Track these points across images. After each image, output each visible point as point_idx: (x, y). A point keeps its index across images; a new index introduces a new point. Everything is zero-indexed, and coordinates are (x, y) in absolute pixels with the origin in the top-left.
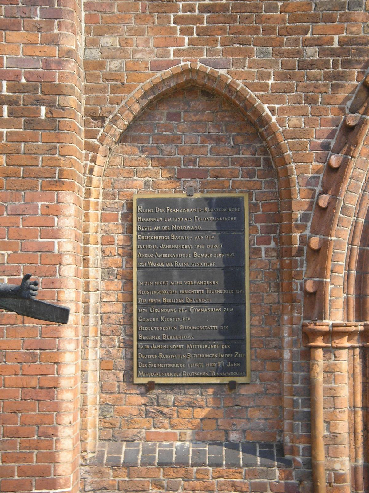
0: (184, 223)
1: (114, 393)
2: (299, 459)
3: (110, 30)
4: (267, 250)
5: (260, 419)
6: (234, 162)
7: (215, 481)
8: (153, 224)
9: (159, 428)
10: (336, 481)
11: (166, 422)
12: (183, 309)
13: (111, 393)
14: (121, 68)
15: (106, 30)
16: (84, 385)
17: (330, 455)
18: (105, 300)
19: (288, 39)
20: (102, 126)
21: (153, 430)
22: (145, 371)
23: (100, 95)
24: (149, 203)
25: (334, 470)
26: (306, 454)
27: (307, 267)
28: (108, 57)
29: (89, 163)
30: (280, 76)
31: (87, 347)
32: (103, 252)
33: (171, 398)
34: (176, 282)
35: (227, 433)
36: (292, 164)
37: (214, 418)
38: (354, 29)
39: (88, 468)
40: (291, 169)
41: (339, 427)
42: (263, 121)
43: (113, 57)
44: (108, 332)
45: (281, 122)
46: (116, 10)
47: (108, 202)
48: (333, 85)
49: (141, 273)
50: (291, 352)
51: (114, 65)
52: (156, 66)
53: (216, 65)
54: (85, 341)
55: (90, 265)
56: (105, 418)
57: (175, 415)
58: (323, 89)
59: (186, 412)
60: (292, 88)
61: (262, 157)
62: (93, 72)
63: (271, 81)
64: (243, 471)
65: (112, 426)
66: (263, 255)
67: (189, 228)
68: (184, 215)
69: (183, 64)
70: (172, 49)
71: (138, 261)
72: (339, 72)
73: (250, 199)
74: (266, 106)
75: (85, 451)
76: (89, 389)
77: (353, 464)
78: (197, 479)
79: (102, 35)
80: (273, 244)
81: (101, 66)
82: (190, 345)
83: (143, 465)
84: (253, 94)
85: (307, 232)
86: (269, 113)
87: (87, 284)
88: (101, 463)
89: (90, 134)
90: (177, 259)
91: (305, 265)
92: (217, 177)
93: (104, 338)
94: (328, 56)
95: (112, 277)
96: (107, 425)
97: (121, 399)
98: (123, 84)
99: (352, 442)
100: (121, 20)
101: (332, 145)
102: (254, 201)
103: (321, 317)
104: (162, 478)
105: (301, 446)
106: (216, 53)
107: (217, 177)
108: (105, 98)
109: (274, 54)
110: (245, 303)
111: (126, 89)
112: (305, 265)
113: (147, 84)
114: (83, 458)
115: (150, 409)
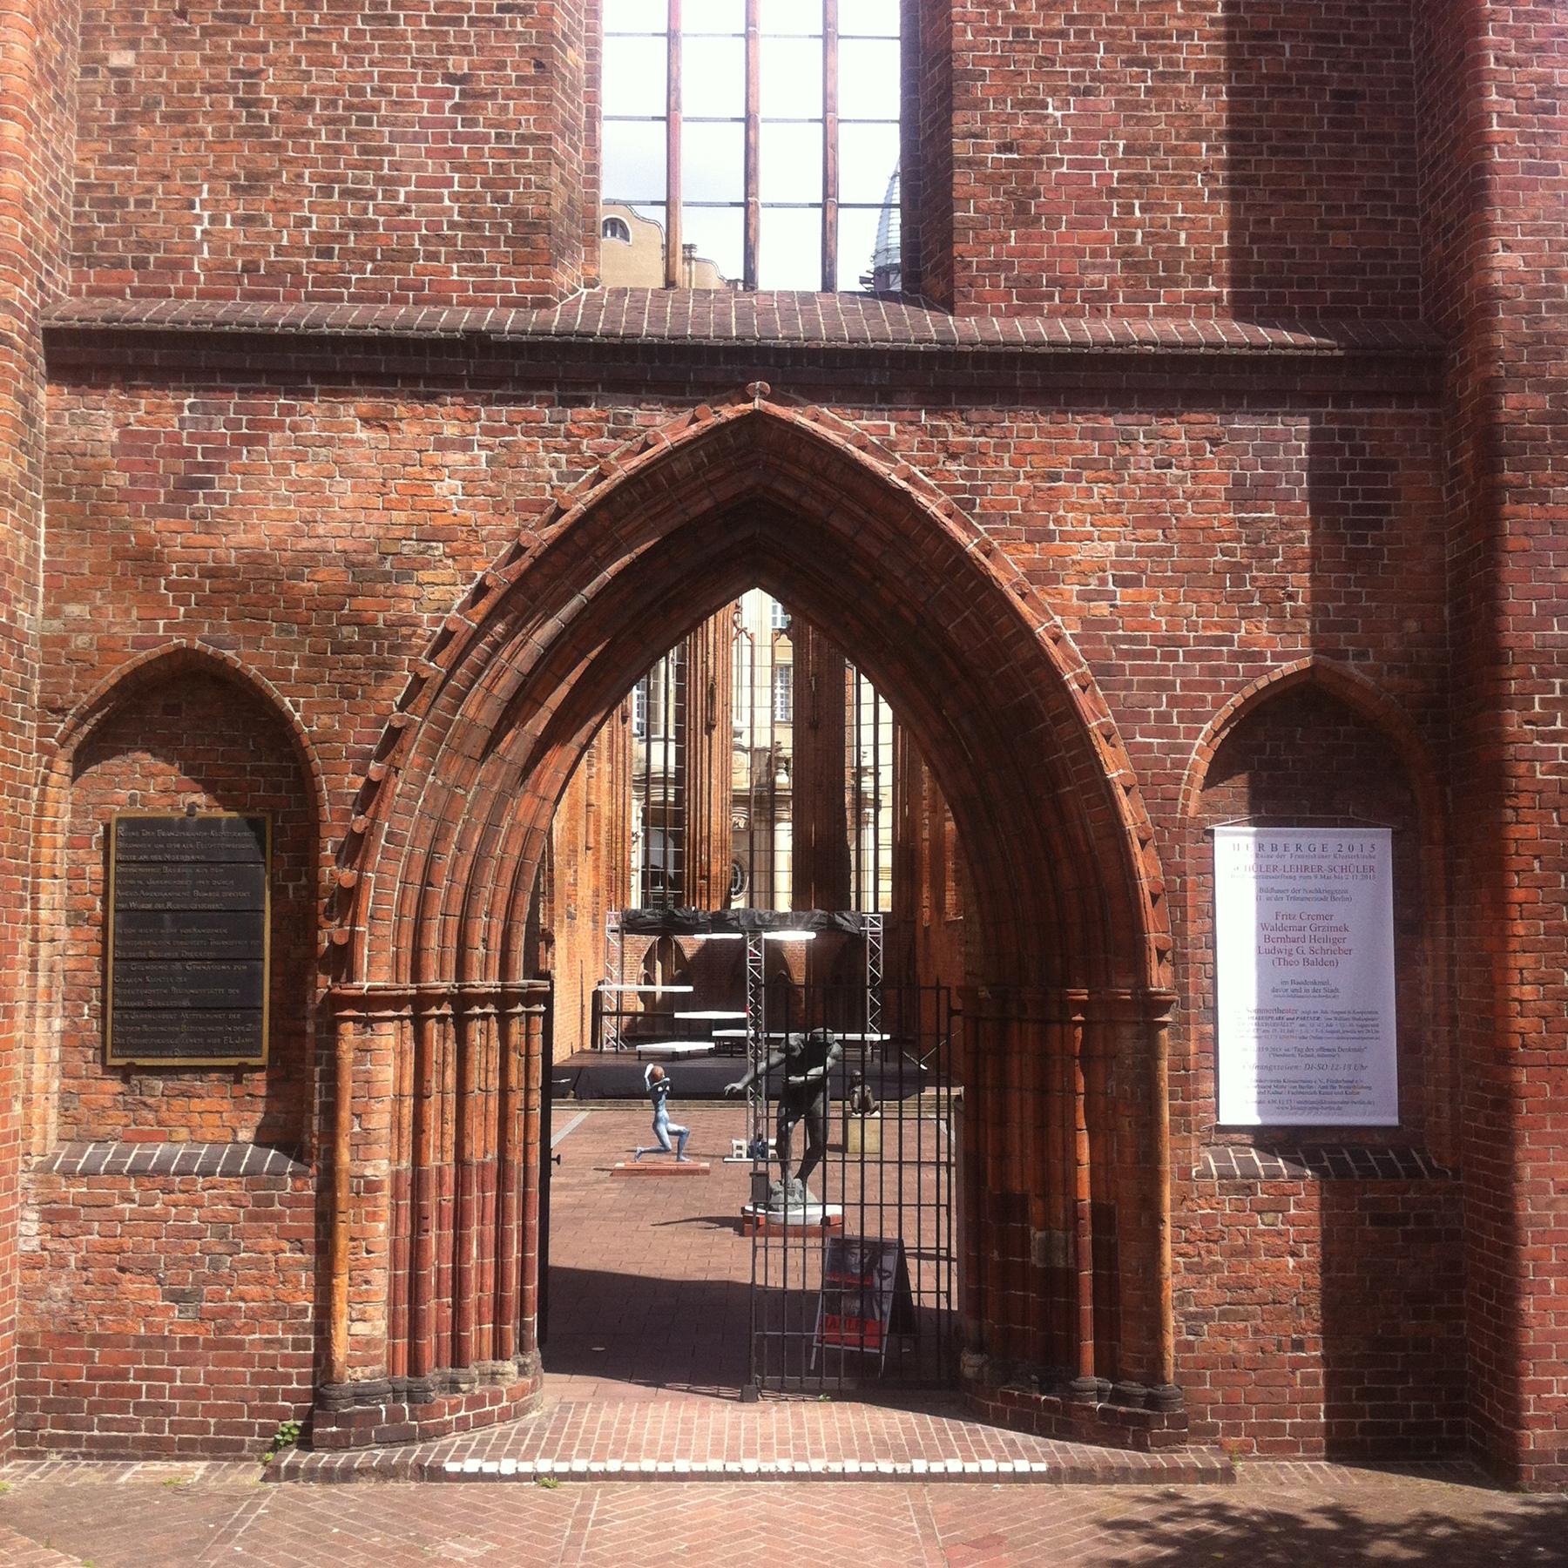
0: (182, 852)
1: (81, 1078)
3: (77, 598)
5: (280, 1112)
6: (256, 771)
7: (206, 1194)
8: (139, 852)
9: (142, 1124)
10: (367, 1190)
11: (151, 1116)
12: (178, 965)
13: (75, 1078)
14: (91, 644)
15: (72, 595)
16: (29, 1066)
17: (361, 1157)
18: (70, 952)
20: (62, 721)
21: (133, 1127)
22: (122, 1048)
23: (61, 680)
24: (133, 824)
25: (363, 1177)
28: (74, 631)
29: (42, 769)
30: (308, 662)
31: (34, 1016)
32: (70, 888)
33: (159, 1085)
34: (169, 929)
35: (235, 1132)
37: (217, 1112)
38: (403, 606)
39: (32, 1176)
40: (320, 782)
41: (373, 1121)
42: (283, 720)
43: (81, 631)
44: (73, 996)
45: (308, 721)
46: (86, 571)
47: (77, 821)
49: (120, 916)
50: (316, 1024)
51: (80, 641)
52: (140, 644)
53: (220, 645)
54: (31, 1008)
55: (41, 905)
56: (67, 1110)
57: (164, 1107)
59: (179, 1103)
60: (322, 677)
62: (53, 649)
63: (296, 667)
64: (244, 1180)
65: (77, 1121)
67: (187, 858)
68: (182, 840)
69: (176, 641)
70: (161, 623)
71: (117, 901)
73: (274, 820)
74: (287, 700)
75: (29, 1154)
76: (36, 1073)
77: (394, 1168)
78: (183, 1192)
79: (67, 603)
81: (63, 641)
82: (185, 1015)
83: (107, 1172)
84: (270, 684)
87: (35, 932)
88: (50, 1169)
89: (45, 731)
90: (170, 899)
92: (229, 791)
93: (67, 1003)
95: (80, 922)
96: (69, 1120)
97: (89, 1086)
98: (92, 665)
99: (395, 1140)
100: (93, 585)
102: (280, 824)
103: (350, 979)
104: (133, 1189)
106: (221, 628)
107: (229, 791)
108: (67, 684)
109: (300, 633)
110: (263, 960)
111: (97, 673)
113: (126, 666)
114: (26, 1162)
115: (129, 1099)
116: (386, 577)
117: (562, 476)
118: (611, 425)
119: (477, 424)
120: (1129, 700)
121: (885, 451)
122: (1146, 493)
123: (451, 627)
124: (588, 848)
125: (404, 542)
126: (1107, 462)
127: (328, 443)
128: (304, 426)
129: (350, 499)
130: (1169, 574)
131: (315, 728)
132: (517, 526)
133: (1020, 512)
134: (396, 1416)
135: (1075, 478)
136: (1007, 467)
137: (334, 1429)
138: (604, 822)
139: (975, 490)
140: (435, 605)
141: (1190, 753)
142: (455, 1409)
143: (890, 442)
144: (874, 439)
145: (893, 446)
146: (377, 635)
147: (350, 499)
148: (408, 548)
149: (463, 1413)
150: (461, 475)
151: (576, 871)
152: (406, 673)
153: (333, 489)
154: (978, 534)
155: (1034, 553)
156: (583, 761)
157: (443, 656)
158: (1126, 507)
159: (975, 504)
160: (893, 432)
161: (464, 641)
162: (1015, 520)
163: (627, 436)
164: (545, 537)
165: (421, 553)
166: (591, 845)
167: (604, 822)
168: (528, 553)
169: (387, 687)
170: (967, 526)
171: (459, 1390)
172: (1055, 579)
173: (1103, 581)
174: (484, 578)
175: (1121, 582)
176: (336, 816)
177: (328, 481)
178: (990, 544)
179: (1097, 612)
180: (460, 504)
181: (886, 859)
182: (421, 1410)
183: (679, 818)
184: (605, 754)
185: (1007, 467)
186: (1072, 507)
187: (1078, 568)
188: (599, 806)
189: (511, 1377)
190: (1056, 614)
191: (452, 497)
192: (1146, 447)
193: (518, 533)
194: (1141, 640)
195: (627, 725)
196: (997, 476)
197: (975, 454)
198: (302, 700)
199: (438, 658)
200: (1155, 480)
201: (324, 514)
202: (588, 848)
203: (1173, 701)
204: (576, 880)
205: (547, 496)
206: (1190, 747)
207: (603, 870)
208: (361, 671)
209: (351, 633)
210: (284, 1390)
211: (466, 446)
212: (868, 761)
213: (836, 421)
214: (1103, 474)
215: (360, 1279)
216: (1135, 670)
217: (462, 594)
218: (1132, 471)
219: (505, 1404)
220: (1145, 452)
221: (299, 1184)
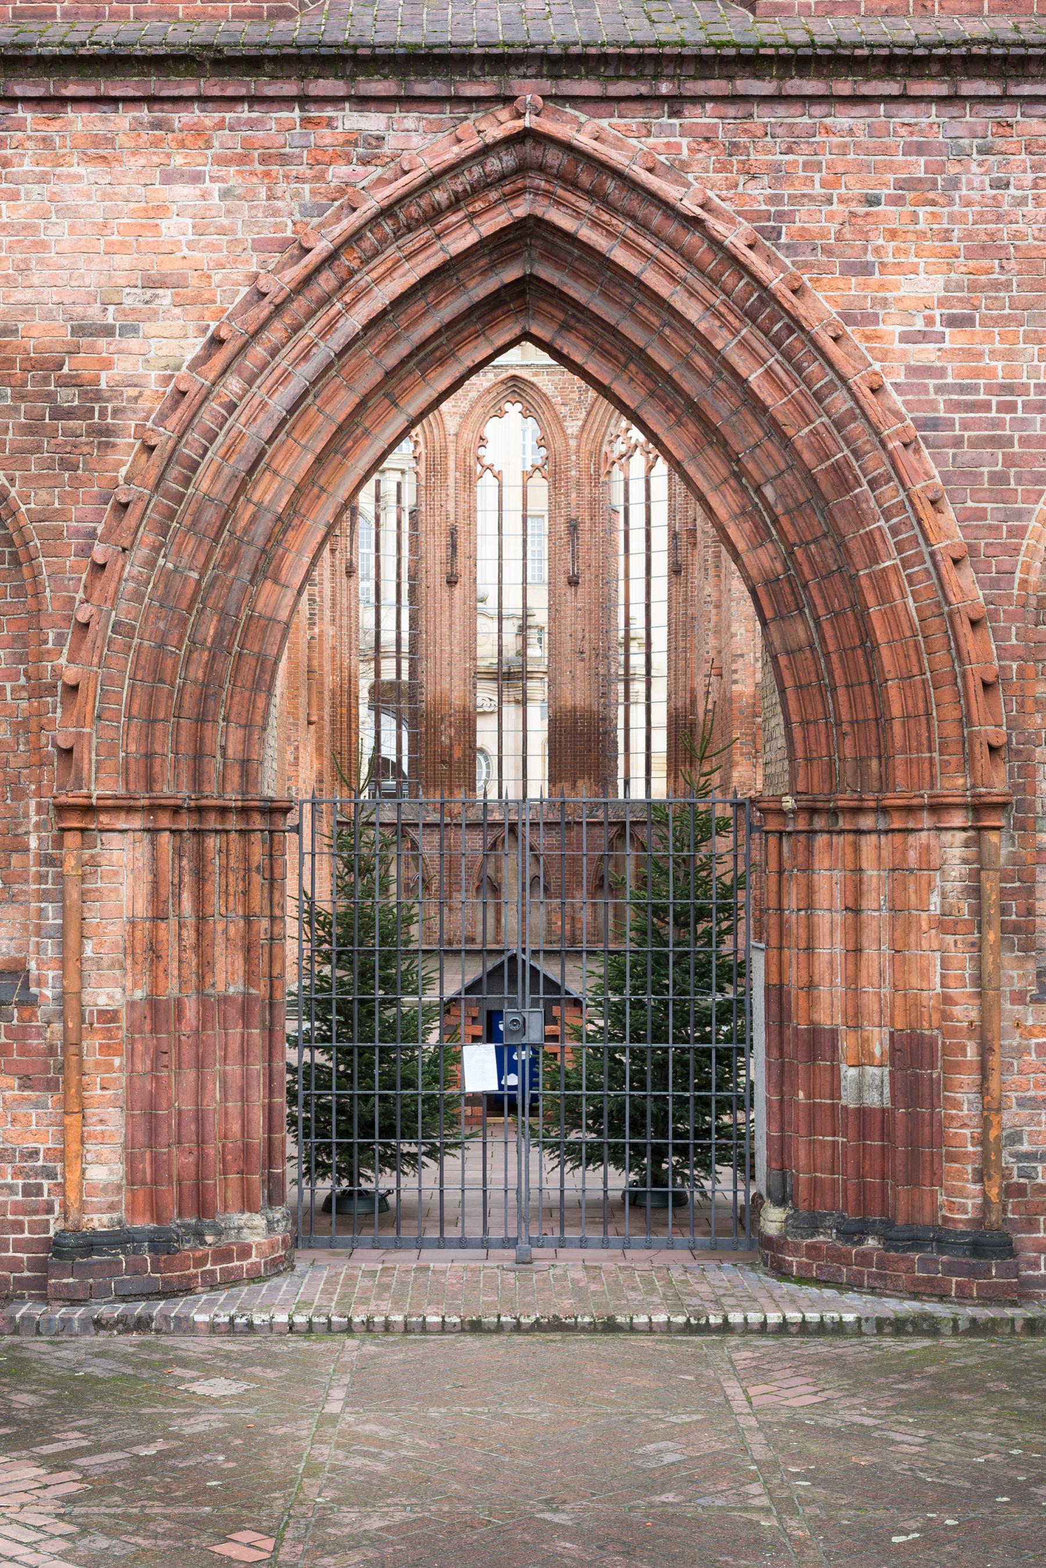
2: (48, 992)
4: (13, 690)
19: (33, 377)
26: (58, 985)
27: (63, 713)
35: (499, 1316)
36: (41, 559)
48: (99, 443)
50: (39, 838)
58: (86, 449)
61: (7, 550)
66: (9, 697)
72: (107, 425)
80: (23, 681)
85: (63, 661)
86: (7, 484)
91: (59, 710)
94: (91, 400)
101: (99, 531)
105: (51, 974)
112: (59, 710)
116: (107, 331)
117: (305, 211)
118: (360, 150)
119: (209, 152)
120: (959, 459)
121: (677, 170)
122: (980, 219)
123: (182, 387)
124: (310, 723)
125: (128, 290)
126: (935, 182)
127: (43, 179)
128: (15, 161)
129: (68, 241)
130: (1007, 311)
131: (32, 506)
132: (254, 269)
133: (832, 241)
134: (136, 1269)
135: (897, 201)
136: (818, 190)
137: (71, 1280)
138: (327, 695)
139: (780, 216)
140: (163, 363)
141: (1029, 520)
142: (200, 1262)
143: (682, 162)
144: (662, 158)
145: (685, 166)
146: (98, 397)
147: (68, 241)
148: (131, 299)
149: (208, 1267)
150: (191, 211)
151: (297, 748)
152: (132, 440)
153: (48, 232)
154: (784, 268)
155: (853, 287)
156: (326, 553)
157: (173, 421)
158: (955, 234)
159: (780, 234)
160: (685, 151)
161: (196, 401)
162: (827, 251)
163: (378, 162)
164: (287, 279)
165: (147, 303)
166: (314, 718)
167: (327, 695)
168: (267, 299)
169: (112, 457)
170: (770, 259)
171: (203, 1243)
172: (874, 319)
173: (930, 321)
174: (218, 328)
175: (952, 321)
176: (57, 604)
177: (42, 222)
178: (798, 279)
179: (923, 356)
180: (190, 246)
181: (660, 742)
182: (165, 1261)
183: (414, 690)
184: (328, 614)
185: (818, 190)
186: (893, 234)
187: (900, 306)
188: (321, 675)
189: (260, 1231)
190: (876, 359)
191: (181, 237)
192: (980, 165)
193: (256, 277)
194: (973, 389)
195: (353, 581)
196: (806, 200)
197: (778, 174)
198: (17, 473)
199: (167, 423)
200: (990, 202)
201: (40, 261)
202: (310, 723)
203: (1010, 461)
204: (297, 758)
205: (289, 234)
206: (1030, 512)
207: (327, 751)
208: (83, 439)
209: (70, 398)
210: (14, 1240)
211: (197, 178)
212: (638, 629)
213: (620, 139)
214: (931, 195)
215: (95, 1119)
216: (965, 426)
217: (195, 346)
218: (964, 192)
219: (254, 1259)
220: (978, 170)
221: (26, 1015)
